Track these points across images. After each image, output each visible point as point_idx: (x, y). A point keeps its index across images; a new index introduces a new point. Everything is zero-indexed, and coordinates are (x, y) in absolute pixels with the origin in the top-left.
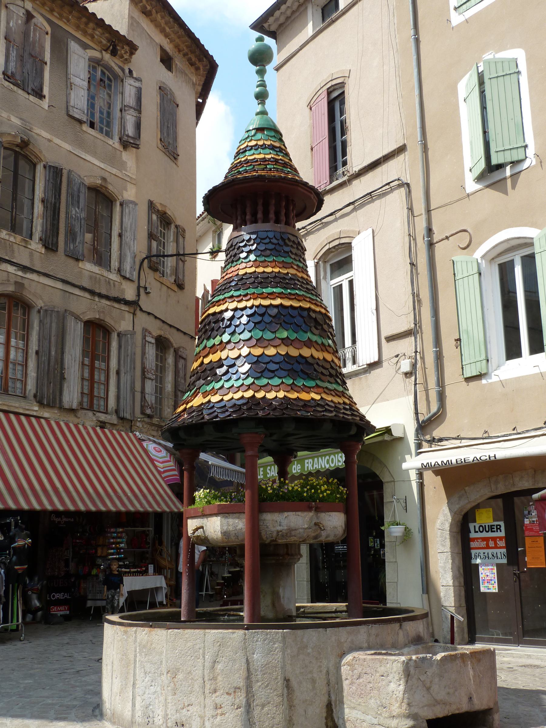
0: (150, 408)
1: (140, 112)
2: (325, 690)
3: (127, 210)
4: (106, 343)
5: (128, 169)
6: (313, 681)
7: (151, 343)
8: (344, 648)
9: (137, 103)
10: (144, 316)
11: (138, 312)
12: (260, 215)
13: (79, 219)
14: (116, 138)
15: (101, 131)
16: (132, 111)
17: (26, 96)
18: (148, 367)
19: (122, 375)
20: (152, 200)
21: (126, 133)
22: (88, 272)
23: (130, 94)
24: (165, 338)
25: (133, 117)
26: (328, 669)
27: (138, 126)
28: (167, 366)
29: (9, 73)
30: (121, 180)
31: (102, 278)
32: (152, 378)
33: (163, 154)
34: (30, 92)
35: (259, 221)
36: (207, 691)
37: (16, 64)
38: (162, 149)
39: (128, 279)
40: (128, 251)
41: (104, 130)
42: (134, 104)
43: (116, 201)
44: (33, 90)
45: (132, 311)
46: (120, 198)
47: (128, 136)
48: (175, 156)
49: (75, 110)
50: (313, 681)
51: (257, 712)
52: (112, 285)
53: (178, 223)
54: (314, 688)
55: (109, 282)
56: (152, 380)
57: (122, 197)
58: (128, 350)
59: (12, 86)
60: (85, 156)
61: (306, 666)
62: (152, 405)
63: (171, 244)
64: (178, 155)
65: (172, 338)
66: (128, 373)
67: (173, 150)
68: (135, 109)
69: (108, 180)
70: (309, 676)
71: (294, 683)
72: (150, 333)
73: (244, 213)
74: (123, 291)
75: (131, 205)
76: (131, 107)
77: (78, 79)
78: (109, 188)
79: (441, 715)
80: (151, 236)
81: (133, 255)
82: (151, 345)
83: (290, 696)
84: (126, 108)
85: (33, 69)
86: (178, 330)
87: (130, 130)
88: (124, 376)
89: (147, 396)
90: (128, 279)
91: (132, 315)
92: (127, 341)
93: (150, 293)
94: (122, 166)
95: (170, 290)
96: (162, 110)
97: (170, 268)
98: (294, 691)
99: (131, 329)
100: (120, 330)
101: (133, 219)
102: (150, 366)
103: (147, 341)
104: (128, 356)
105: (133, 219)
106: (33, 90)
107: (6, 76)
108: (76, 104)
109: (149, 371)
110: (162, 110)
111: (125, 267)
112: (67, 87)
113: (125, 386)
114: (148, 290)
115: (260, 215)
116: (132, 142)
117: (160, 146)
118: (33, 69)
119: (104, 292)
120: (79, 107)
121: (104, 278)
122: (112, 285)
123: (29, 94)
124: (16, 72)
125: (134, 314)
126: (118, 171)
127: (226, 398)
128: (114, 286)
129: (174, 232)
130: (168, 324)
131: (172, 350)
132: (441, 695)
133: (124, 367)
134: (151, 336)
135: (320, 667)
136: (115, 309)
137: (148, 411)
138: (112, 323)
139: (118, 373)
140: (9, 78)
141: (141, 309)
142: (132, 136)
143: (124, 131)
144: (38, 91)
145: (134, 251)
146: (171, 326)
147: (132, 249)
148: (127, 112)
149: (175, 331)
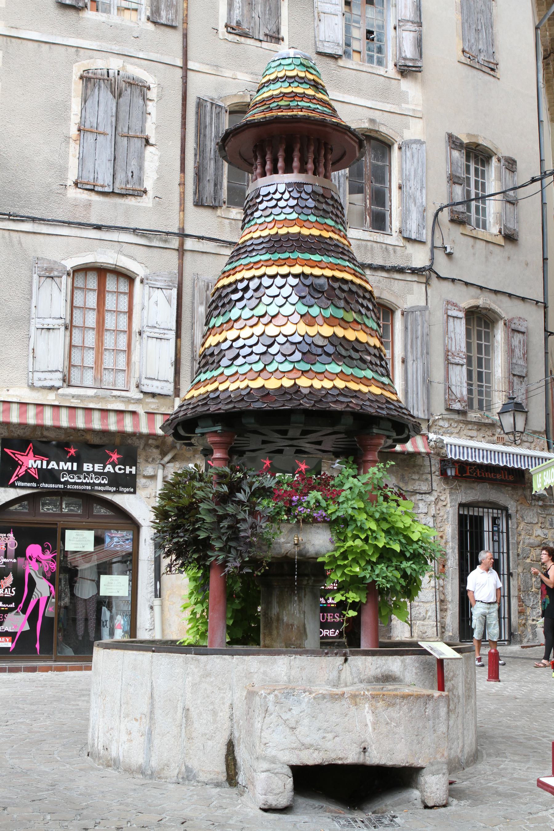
0: (459, 401)
1: (420, 24)
2: (228, 724)
3: (408, 154)
4: (388, 325)
5: (410, 99)
6: (214, 713)
7: (457, 318)
8: (254, 680)
9: (415, 13)
10: (447, 285)
11: (434, 280)
12: (280, 164)
13: (337, 178)
14: (391, 65)
15: (371, 59)
16: (409, 26)
17: (258, 44)
18: (453, 349)
19: (410, 362)
20: (450, 132)
21: (403, 55)
22: (355, 241)
23: (405, 4)
24: (486, 309)
25: (412, 33)
26: (233, 700)
27: (419, 44)
28: (496, 344)
29: (234, 24)
30: (400, 116)
31: (375, 245)
32: (461, 362)
33: (470, 68)
34: (261, 38)
35: (268, 174)
36: (122, 716)
37: (243, 10)
38: (468, 61)
39: (415, 241)
40: (413, 205)
41: (375, 57)
42: (412, 15)
43: (393, 144)
44: (266, 35)
45: (424, 280)
46: (398, 139)
47: (405, 59)
48: (492, 66)
49: (326, 44)
50: (214, 713)
51: (156, 742)
52: (392, 252)
53: (504, 151)
54: (215, 721)
55: (386, 249)
56: (462, 365)
57: (402, 137)
58: (417, 331)
59: (238, 38)
60: (343, 97)
61: (208, 697)
62: (463, 397)
63: (493, 183)
64: (497, 64)
65: (500, 307)
66: (419, 360)
67: (486, 59)
68: (413, 22)
69: (378, 121)
70: (211, 707)
71: (194, 713)
72: (455, 305)
73: (264, 165)
74: (409, 257)
75: (414, 146)
76: (408, 21)
77: (328, 5)
78: (381, 130)
79: (311, 762)
80: (453, 179)
81: (420, 209)
82: (457, 322)
83: (189, 728)
84: (401, 24)
85: (265, 10)
86: (510, 295)
87: (409, 51)
88: (413, 364)
89: (453, 388)
90: (415, 241)
91: (423, 286)
92: (416, 320)
93: (452, 253)
94: (402, 97)
95: (490, 245)
96: (465, 12)
97: (492, 216)
98: (193, 722)
99: (423, 304)
100: (405, 306)
101: (418, 162)
102: (458, 348)
103: (451, 316)
104: (417, 338)
105: (418, 162)
106: (266, 35)
107: (229, 29)
108: (327, 36)
109: (456, 354)
110: (465, 12)
111: (408, 226)
112: (314, 19)
113: (415, 376)
114: (448, 250)
115: (280, 164)
116: (411, 64)
117: (463, 59)
118: (265, 10)
119: (378, 261)
120: (331, 39)
121: (379, 245)
122: (392, 252)
123: (261, 41)
124: (243, 20)
125: (427, 283)
126: (394, 106)
127: (222, 387)
128: (395, 252)
129: (496, 167)
130: (491, 290)
131: (501, 324)
132: (313, 738)
133: (412, 353)
134: (456, 308)
135: (223, 698)
136: (396, 281)
137: (457, 406)
138: (392, 299)
139: (404, 361)
140: (233, 29)
141: (439, 277)
142: (411, 57)
143: (400, 53)
144: (274, 35)
145: (422, 203)
146: (496, 292)
147: (419, 202)
148: (403, 28)
149: (505, 299)
